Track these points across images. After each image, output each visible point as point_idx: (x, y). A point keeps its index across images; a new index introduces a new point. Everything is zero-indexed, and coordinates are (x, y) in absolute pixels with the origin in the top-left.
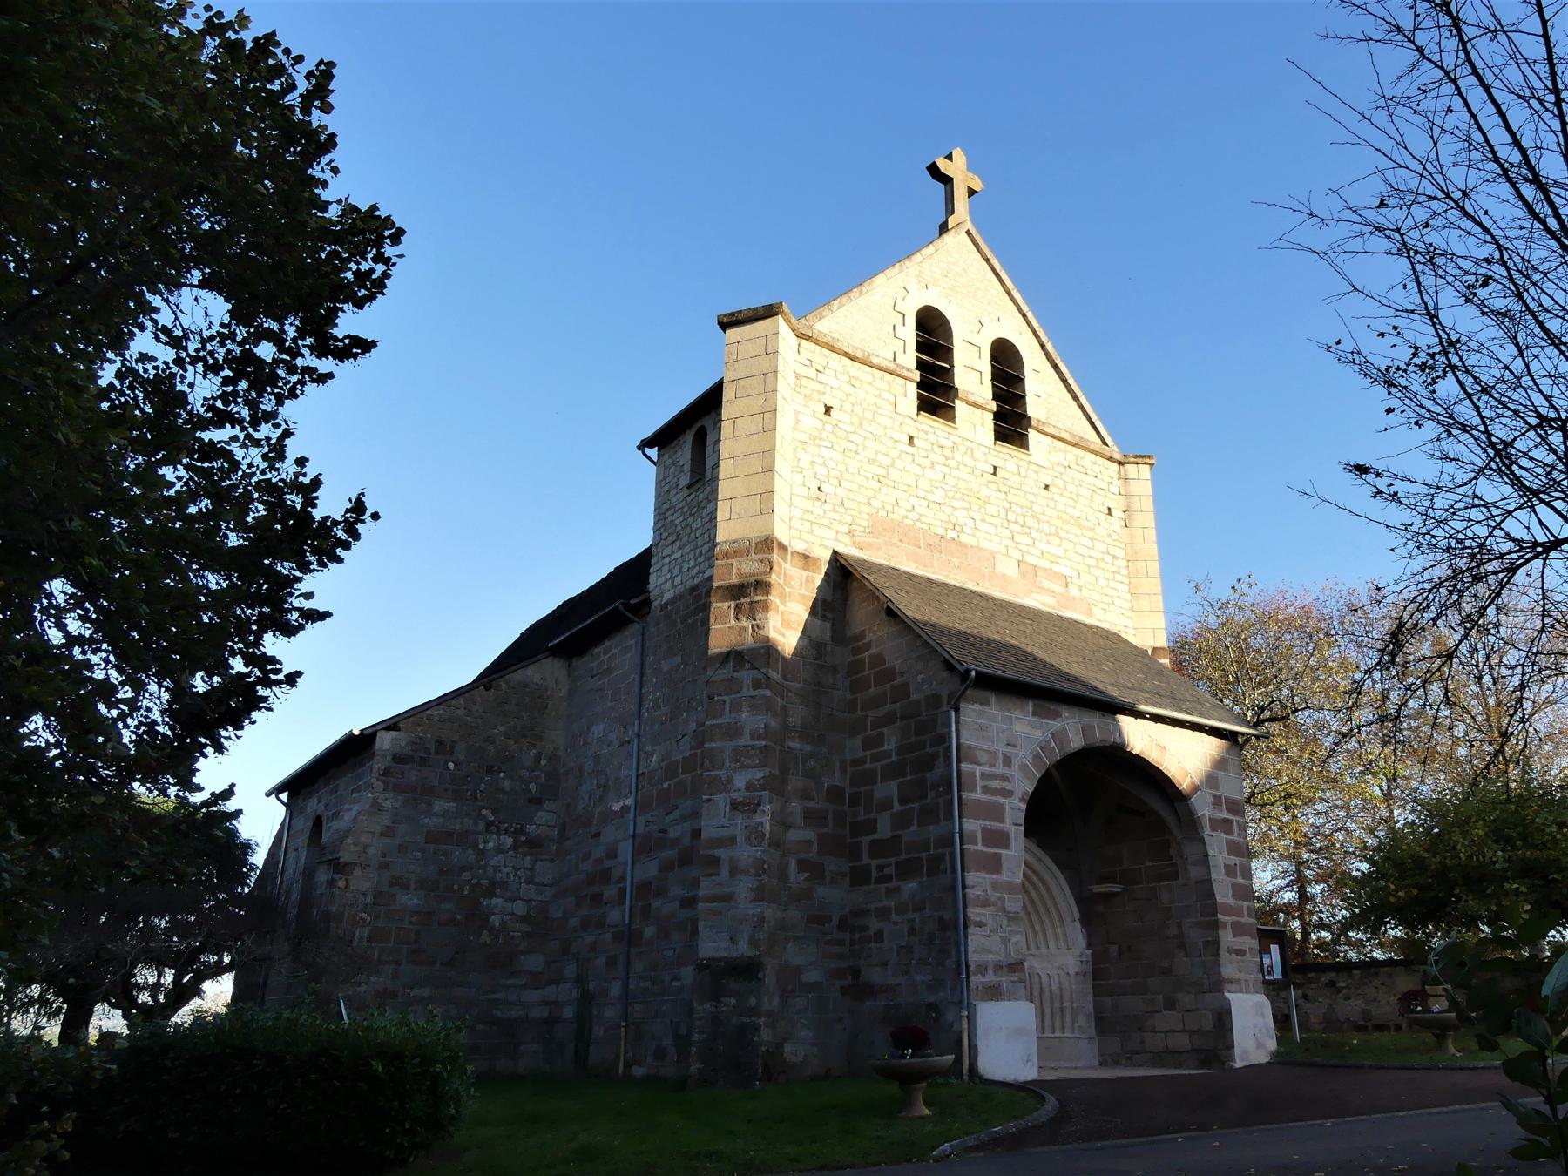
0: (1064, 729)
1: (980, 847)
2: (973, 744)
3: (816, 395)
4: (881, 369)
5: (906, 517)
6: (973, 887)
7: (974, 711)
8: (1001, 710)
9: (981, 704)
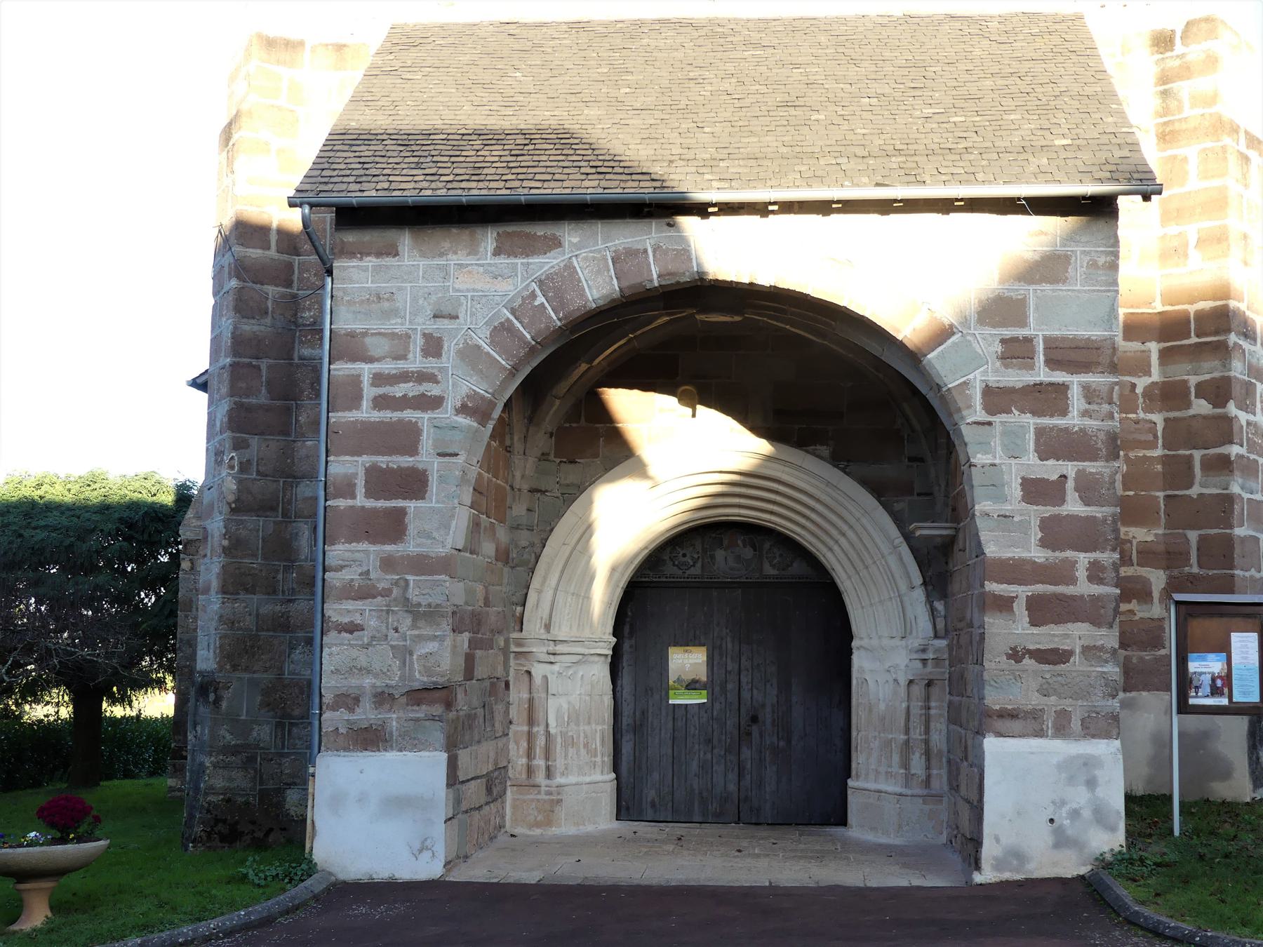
0: (569, 267)
1: (361, 500)
2: (358, 326)
6: (341, 568)
7: (366, 269)
8: (423, 255)
9: (379, 254)
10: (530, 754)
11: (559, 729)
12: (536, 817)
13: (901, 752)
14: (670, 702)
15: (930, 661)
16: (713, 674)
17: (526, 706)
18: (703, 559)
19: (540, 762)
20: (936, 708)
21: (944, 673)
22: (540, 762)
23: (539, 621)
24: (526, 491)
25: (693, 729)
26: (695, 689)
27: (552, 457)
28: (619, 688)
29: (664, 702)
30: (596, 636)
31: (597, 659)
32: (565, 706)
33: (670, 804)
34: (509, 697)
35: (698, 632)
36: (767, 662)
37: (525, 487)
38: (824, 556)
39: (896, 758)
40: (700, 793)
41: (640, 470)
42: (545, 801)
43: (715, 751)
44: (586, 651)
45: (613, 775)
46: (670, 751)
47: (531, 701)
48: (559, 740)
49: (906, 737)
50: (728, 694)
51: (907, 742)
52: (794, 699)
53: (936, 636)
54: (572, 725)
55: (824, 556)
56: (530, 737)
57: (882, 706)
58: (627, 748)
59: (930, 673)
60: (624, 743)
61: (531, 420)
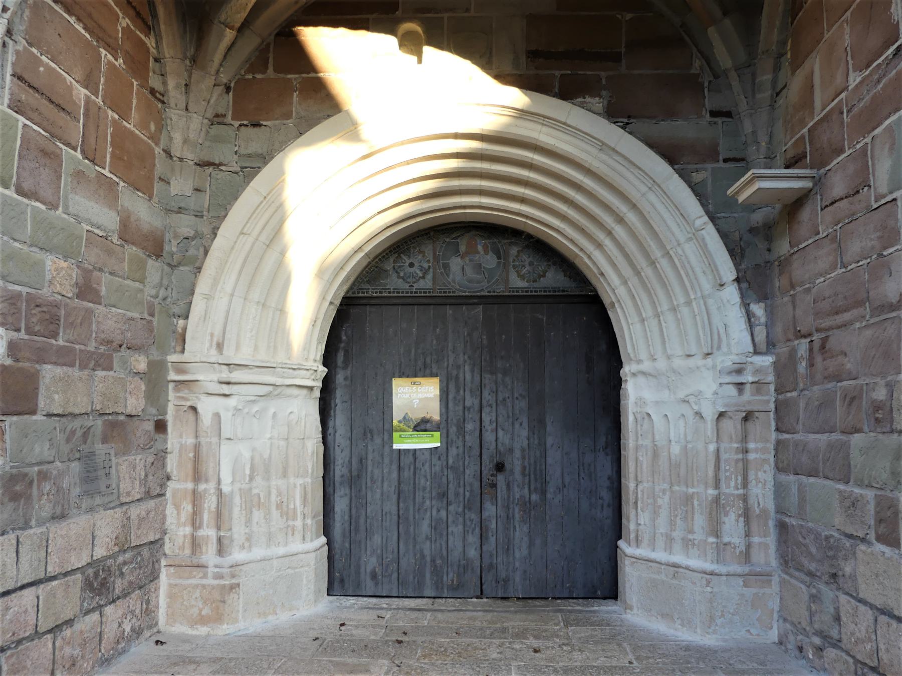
10: (195, 521)
11: (237, 485)
12: (201, 610)
13: (710, 514)
14: (395, 446)
15: (748, 386)
16: (447, 412)
17: (191, 455)
18: (435, 269)
19: (208, 532)
20: (756, 450)
21: (768, 402)
22: (208, 532)
23: (208, 338)
24: (192, 163)
25: (423, 481)
26: (426, 430)
27: (229, 119)
28: (330, 431)
29: (387, 449)
30: (296, 360)
31: (296, 391)
32: (247, 454)
33: (395, 575)
34: (166, 441)
35: (428, 360)
36: (516, 395)
37: (190, 156)
38: (589, 257)
39: (700, 521)
40: (433, 561)
41: (351, 131)
42: (213, 587)
43: (451, 508)
44: (279, 381)
45: (323, 540)
46: (394, 509)
47: (197, 448)
48: (237, 500)
49: (716, 492)
50: (467, 437)
51: (717, 500)
52: (550, 441)
53: (756, 352)
54: (259, 480)
55: (589, 257)
56: (196, 498)
57: (676, 449)
58: (341, 505)
59: (749, 402)
60: (337, 499)
61: (194, 60)
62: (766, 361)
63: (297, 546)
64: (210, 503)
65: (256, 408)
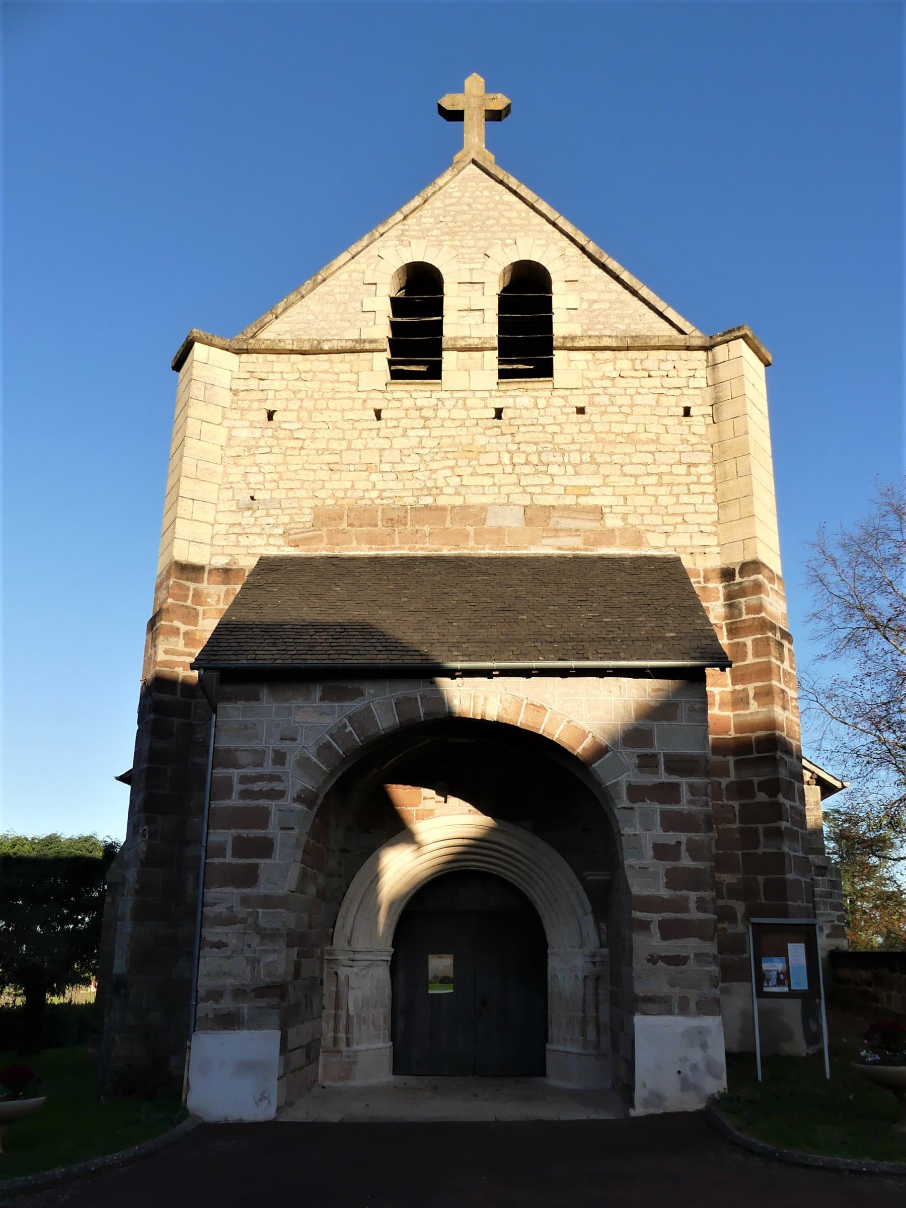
0: (368, 709)
1: (229, 859)
2: (232, 745)
3: (256, 405)
4: (339, 352)
5: (363, 498)
6: (215, 904)
10: (336, 1030)
14: (430, 992)
22: (342, 1035)
44: (374, 958)
45: (391, 1043)
48: (355, 1020)
51: (584, 1018)
56: (336, 1018)
62: (606, 951)
63: (381, 1045)
64: (343, 1021)
65: (364, 972)
